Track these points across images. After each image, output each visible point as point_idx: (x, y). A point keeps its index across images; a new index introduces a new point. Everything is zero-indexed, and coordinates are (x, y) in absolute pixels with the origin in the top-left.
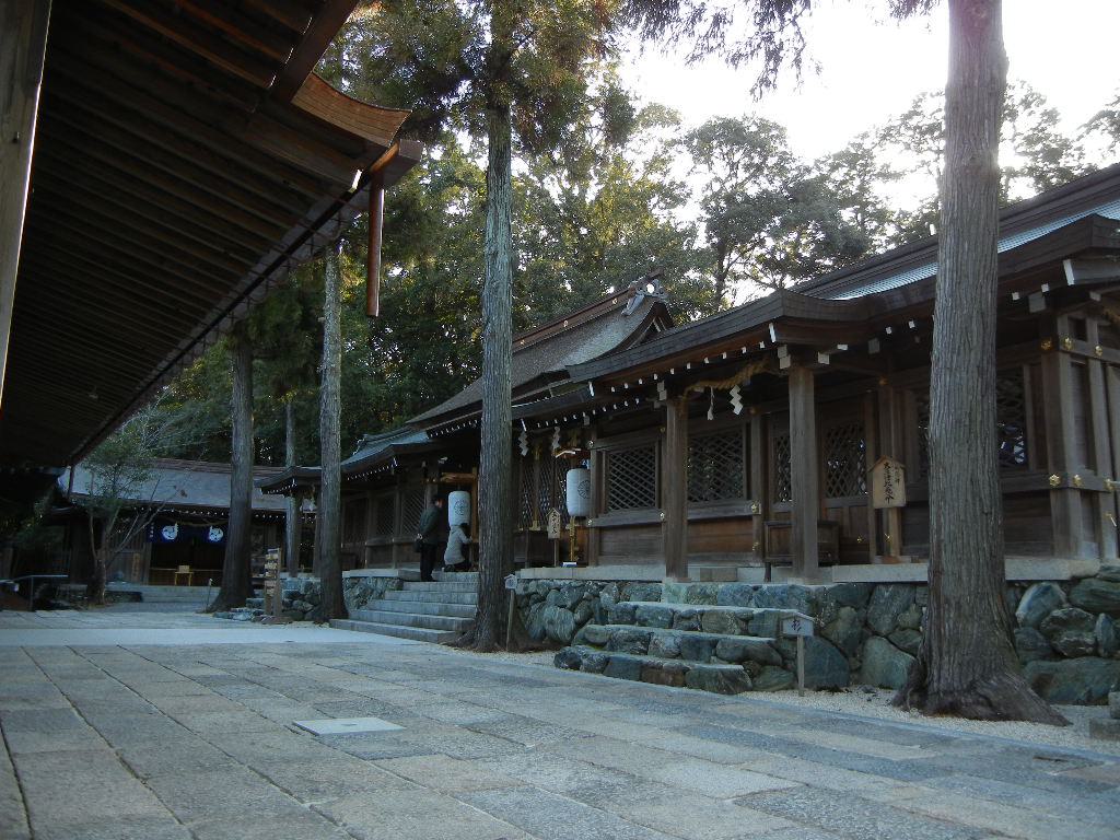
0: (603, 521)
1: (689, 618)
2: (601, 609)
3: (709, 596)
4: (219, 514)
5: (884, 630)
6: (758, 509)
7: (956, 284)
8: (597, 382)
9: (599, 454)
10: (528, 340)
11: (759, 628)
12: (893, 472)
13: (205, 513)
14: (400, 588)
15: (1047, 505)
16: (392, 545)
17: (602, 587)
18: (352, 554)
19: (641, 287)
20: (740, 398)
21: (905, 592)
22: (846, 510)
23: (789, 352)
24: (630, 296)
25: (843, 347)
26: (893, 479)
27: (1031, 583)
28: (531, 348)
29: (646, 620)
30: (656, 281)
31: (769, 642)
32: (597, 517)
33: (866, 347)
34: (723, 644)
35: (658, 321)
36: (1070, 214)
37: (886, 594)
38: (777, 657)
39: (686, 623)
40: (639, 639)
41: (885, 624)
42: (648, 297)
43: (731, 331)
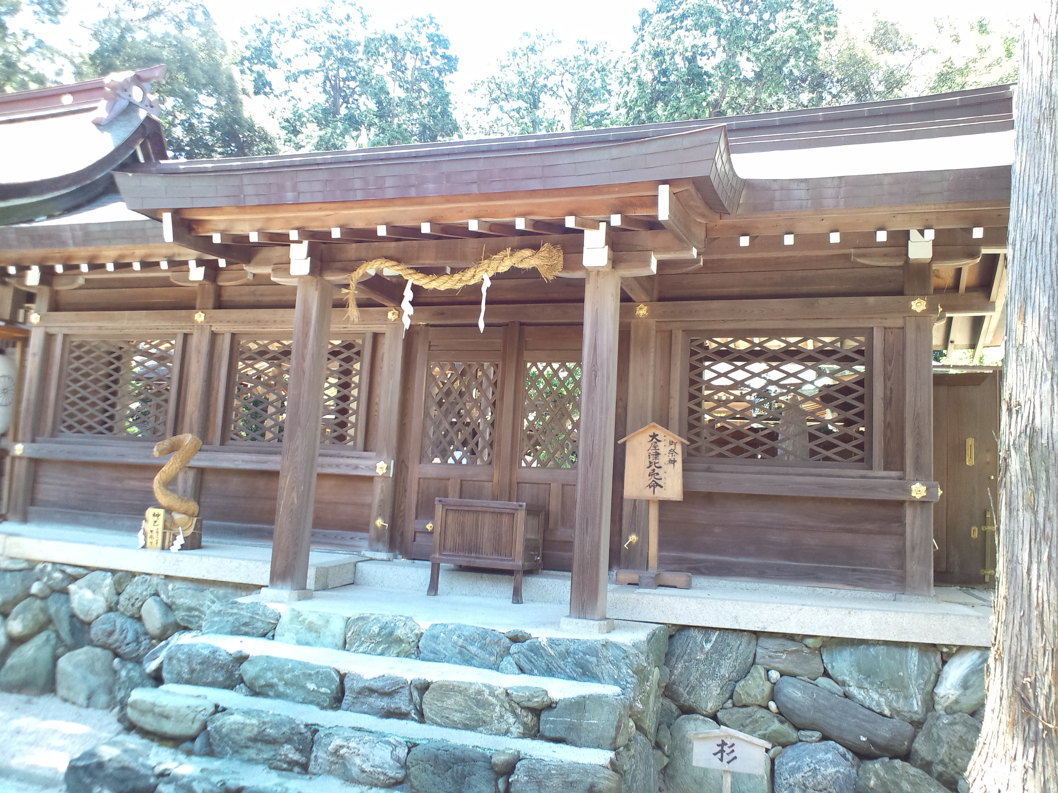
0: (43, 449)
1: (390, 694)
2: (73, 616)
3: (399, 641)
5: (710, 706)
6: (388, 468)
11: (571, 727)
12: (663, 448)
15: (900, 520)
17: (74, 579)
21: (742, 647)
22: (555, 487)
26: (663, 460)
27: (962, 649)
29: (271, 686)
32: (33, 441)
33: (970, 231)
34: (530, 772)
35: (143, 146)
36: (84, 227)
37: (708, 646)
39: (383, 703)
40: (289, 741)
41: (710, 696)
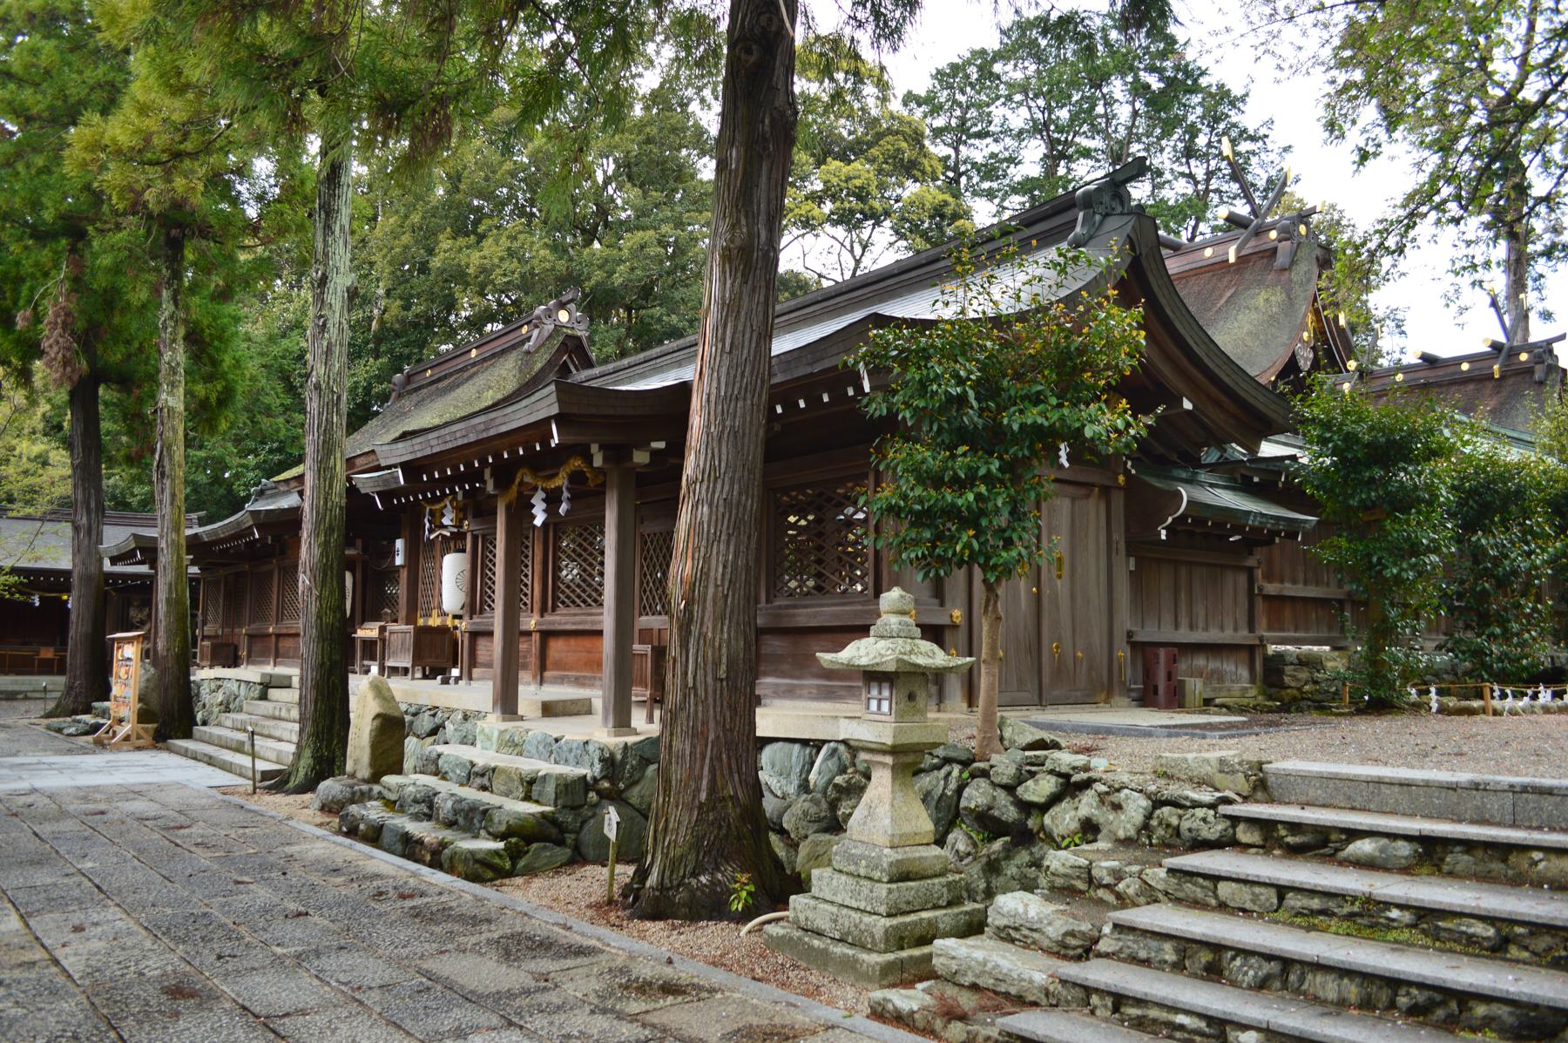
4: (57, 579)
7: (723, 404)
8: (405, 466)
9: (475, 538)
10: (437, 370)
13: (47, 578)
14: (263, 697)
16: (269, 635)
18: (228, 645)
19: (549, 314)
20: (544, 506)
23: (601, 448)
24: (536, 326)
25: (661, 445)
27: (824, 742)
28: (485, 360)
30: (572, 306)
31: (543, 815)
38: (554, 831)
39: (479, 781)
42: (558, 328)
43: (504, 429)
